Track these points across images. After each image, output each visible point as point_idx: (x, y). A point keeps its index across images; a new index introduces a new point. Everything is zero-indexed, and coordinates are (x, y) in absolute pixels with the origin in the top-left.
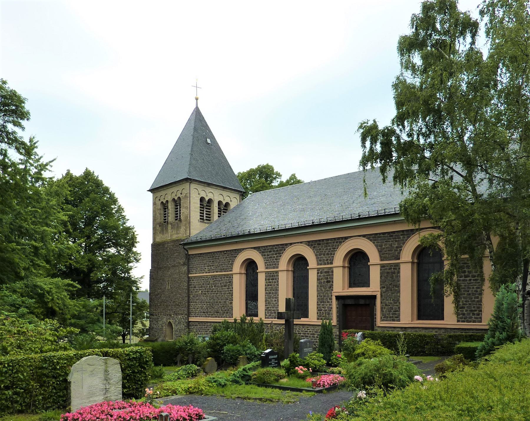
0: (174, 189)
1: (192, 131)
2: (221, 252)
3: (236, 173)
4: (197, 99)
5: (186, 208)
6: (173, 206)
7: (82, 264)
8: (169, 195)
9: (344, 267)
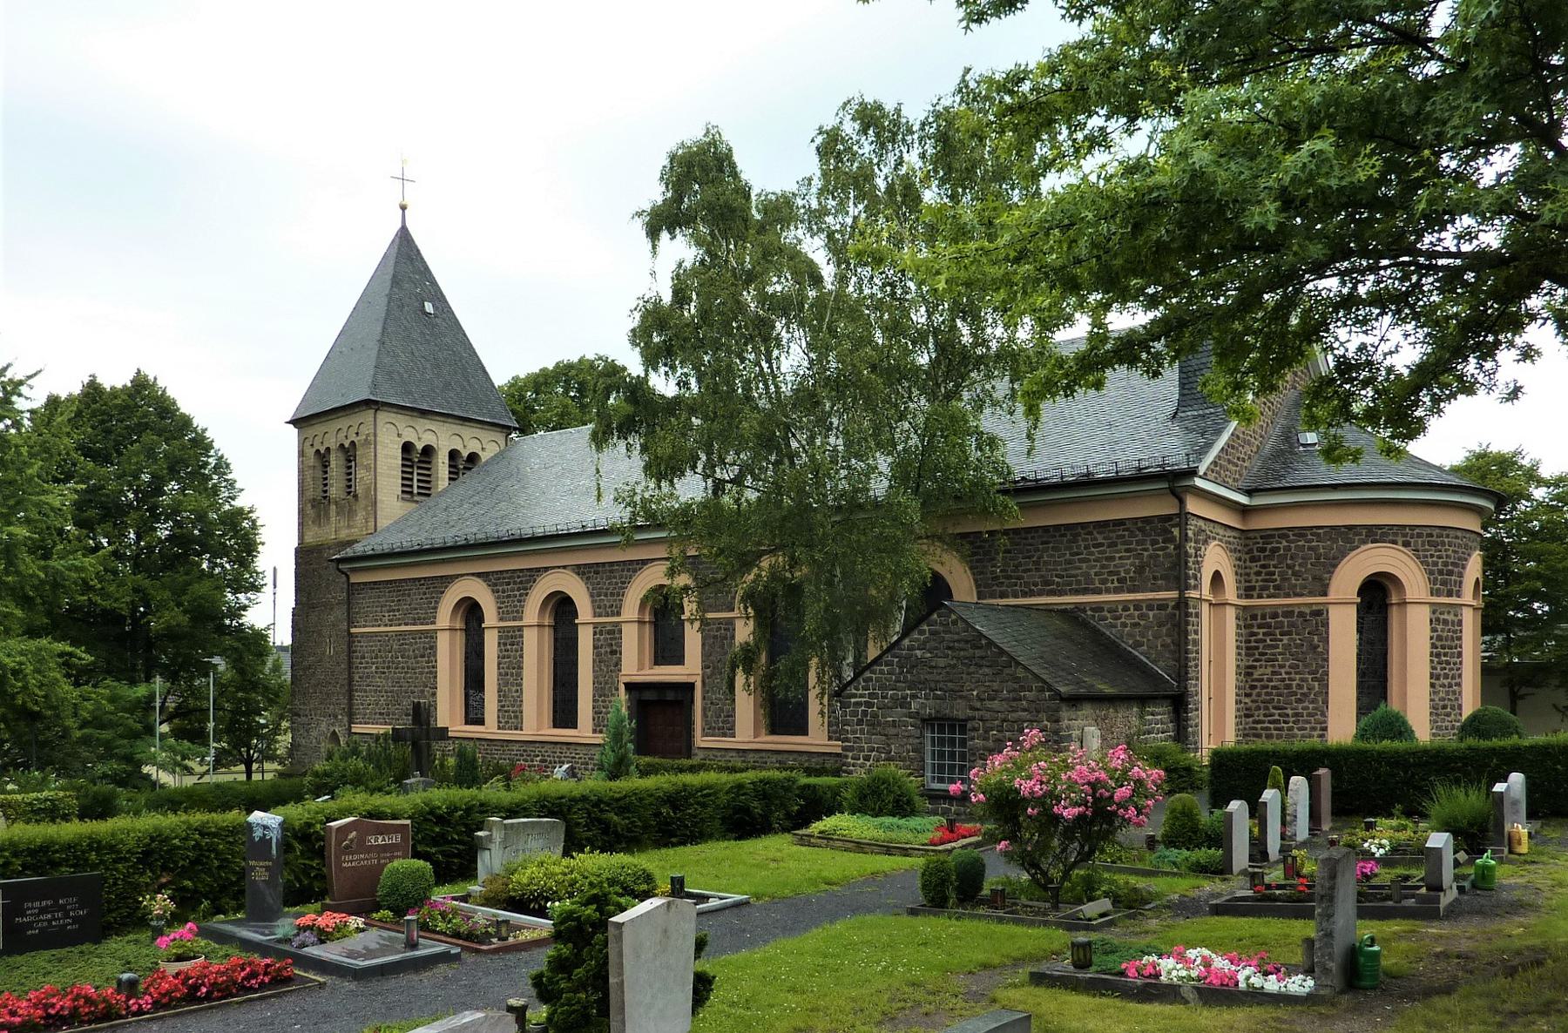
0: (342, 422)
1: (388, 284)
2: (414, 580)
3: (500, 376)
4: (403, 208)
5: (367, 468)
6: (342, 462)
7: (116, 600)
8: (332, 435)
9: (641, 622)
